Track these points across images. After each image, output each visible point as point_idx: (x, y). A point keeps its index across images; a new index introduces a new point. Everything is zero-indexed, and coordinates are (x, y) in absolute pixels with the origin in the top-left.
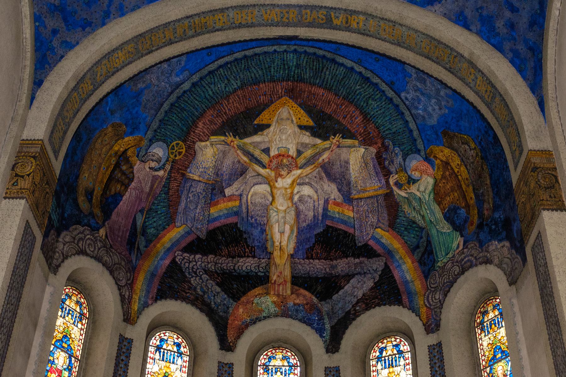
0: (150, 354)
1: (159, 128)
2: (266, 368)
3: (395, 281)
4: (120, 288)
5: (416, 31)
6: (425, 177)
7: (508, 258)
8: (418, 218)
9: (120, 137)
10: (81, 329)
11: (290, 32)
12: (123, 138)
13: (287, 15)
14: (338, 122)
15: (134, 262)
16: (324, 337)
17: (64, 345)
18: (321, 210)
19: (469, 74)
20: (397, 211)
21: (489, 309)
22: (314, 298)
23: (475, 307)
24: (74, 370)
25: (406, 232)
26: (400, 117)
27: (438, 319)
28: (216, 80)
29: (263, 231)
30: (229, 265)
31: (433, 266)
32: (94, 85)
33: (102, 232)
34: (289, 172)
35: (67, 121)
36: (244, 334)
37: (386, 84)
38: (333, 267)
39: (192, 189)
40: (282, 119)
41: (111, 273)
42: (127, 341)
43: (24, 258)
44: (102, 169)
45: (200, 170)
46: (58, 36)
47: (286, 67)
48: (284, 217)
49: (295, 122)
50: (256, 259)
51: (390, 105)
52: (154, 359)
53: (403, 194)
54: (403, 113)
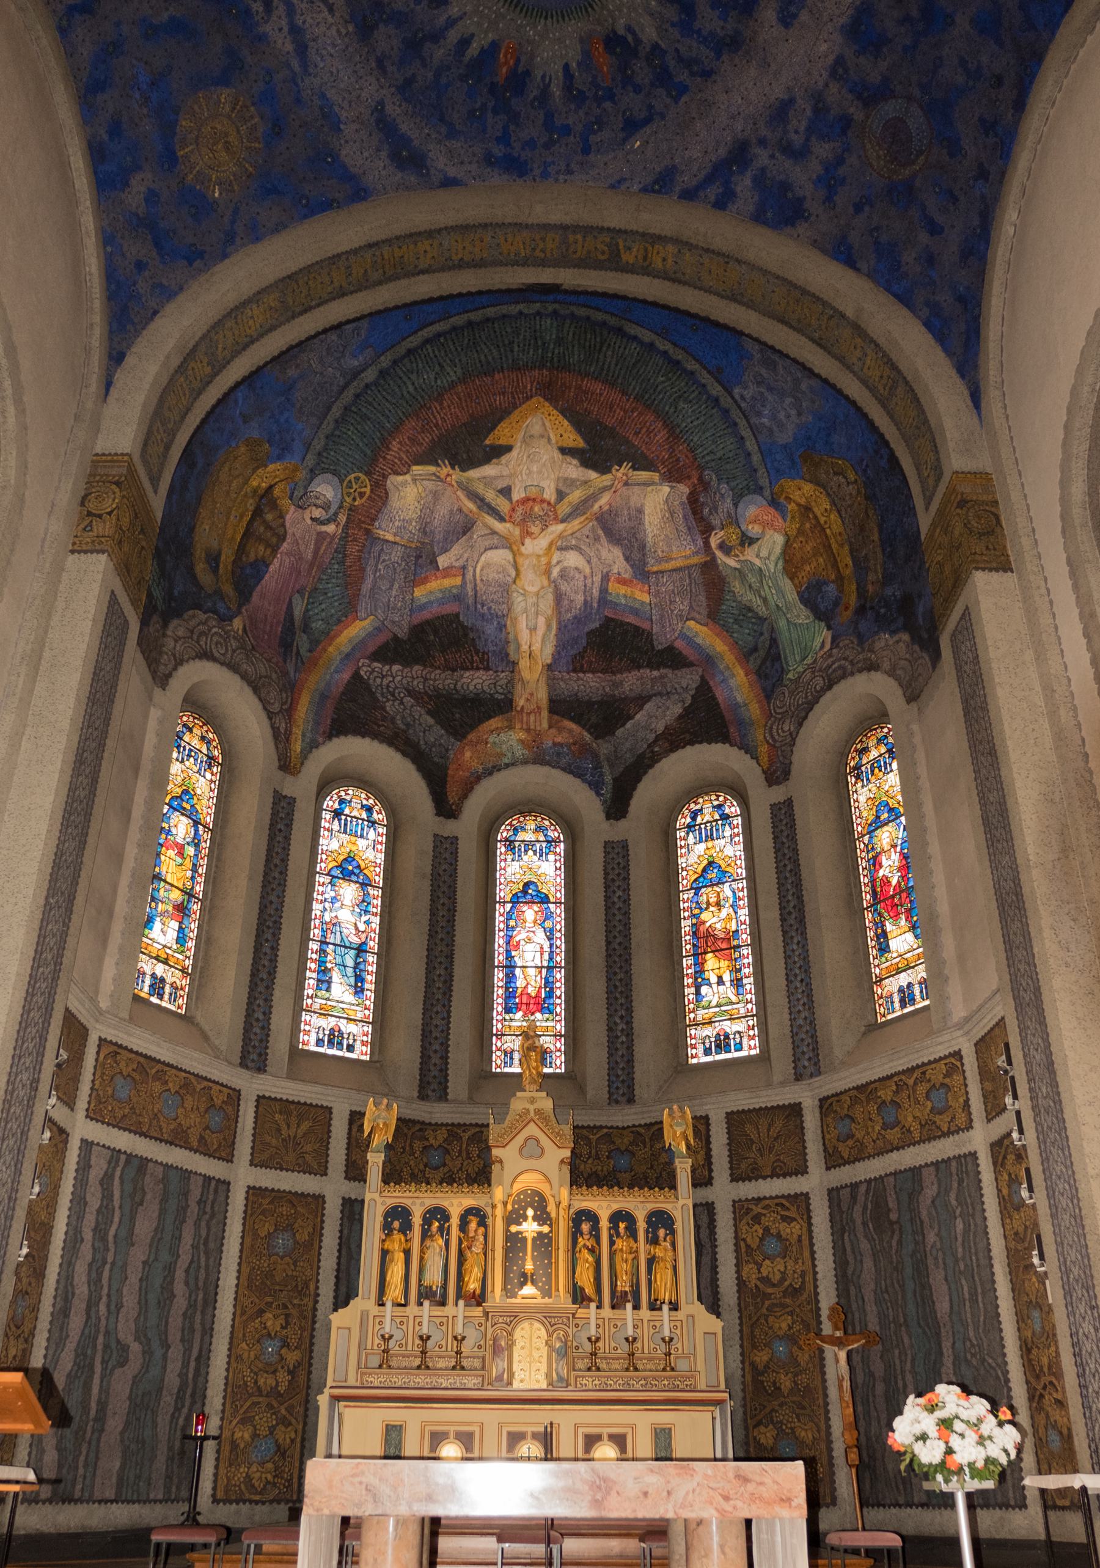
0: (323, 824)
1: (325, 449)
2: (510, 844)
3: (718, 704)
4: (270, 715)
5: (765, 272)
6: (769, 533)
7: (906, 659)
8: (757, 603)
9: (261, 463)
10: (211, 781)
11: (546, 276)
12: (266, 466)
13: (541, 245)
14: (627, 442)
15: (292, 674)
16: (602, 795)
17: (184, 805)
18: (596, 593)
19: (852, 347)
20: (722, 591)
21: (870, 745)
22: (585, 733)
23: (847, 742)
24: (203, 844)
25: (736, 627)
26: (730, 430)
27: (787, 762)
28: (420, 365)
29: (502, 627)
30: (447, 682)
31: (780, 679)
32: (213, 366)
33: (237, 623)
34: (545, 527)
35: (170, 426)
36: (475, 791)
37: (709, 372)
38: (616, 685)
39: (383, 557)
40: (531, 436)
41: (256, 690)
42: (287, 800)
43: (112, 654)
44: (232, 518)
45: (397, 524)
46: (147, 273)
47: (540, 343)
49: (554, 441)
50: (491, 672)
51: (714, 411)
52: (330, 831)
53: (732, 562)
54: (736, 424)
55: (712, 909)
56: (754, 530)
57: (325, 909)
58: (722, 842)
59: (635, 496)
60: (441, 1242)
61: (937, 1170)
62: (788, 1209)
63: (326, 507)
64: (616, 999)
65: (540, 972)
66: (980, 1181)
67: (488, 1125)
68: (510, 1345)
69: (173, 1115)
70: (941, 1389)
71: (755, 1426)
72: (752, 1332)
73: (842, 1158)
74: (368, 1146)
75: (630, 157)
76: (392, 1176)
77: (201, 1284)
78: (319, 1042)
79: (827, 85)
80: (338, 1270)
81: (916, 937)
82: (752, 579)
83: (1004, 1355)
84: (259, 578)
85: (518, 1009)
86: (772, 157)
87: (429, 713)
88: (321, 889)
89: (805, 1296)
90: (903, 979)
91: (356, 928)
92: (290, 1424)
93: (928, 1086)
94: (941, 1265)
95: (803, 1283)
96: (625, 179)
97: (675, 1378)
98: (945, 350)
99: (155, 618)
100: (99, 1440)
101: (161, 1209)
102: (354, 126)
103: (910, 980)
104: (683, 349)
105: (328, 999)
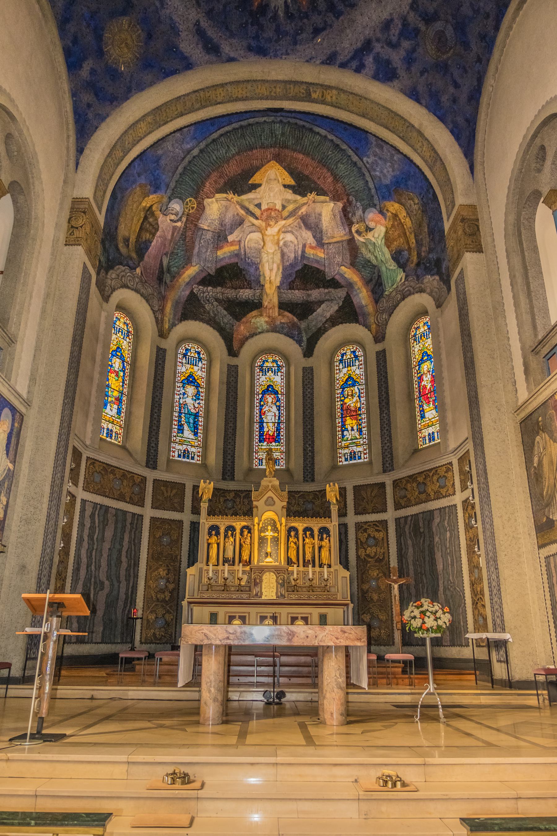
0: (179, 360)
1: (175, 187)
3: (354, 305)
4: (154, 312)
5: (378, 104)
7: (437, 288)
11: (277, 104)
12: (149, 196)
14: (315, 183)
15: (163, 292)
16: (302, 346)
17: (118, 353)
18: (300, 253)
20: (357, 253)
24: (127, 371)
25: (363, 269)
28: (219, 147)
29: (257, 269)
31: (382, 294)
33: (138, 270)
37: (352, 150)
38: (309, 295)
39: (203, 237)
41: (147, 301)
45: (209, 221)
46: (92, 109)
47: (274, 135)
48: (273, 258)
49: (280, 182)
53: (361, 239)
54: (364, 175)
55: (349, 397)
56: (372, 225)
57: (180, 398)
58: (354, 368)
59: (318, 207)
60: (232, 540)
61: (440, 511)
62: (378, 527)
63: (176, 214)
64: (307, 437)
65: (274, 425)
66: (457, 516)
67: (252, 491)
68: (261, 581)
69: (119, 488)
70: (423, 600)
71: (363, 614)
72: (362, 577)
73: (402, 505)
74: (201, 500)
75: (316, 47)
76: (211, 512)
77: (133, 557)
78: (179, 456)
79: (408, 13)
80: (189, 551)
81: (437, 412)
82: (370, 247)
83: (464, 587)
84: (147, 249)
85: (265, 441)
86: (382, 47)
87: (225, 309)
88: (178, 389)
89: (384, 563)
90: (431, 430)
91: (194, 406)
92: (171, 613)
93: (438, 476)
94: (440, 551)
95: (384, 557)
96: (314, 58)
97: (329, 595)
98: (460, 145)
99: (102, 270)
100: (94, 619)
101: (115, 527)
102: (186, 33)
103: (433, 430)
104: (340, 139)
105: (182, 437)
